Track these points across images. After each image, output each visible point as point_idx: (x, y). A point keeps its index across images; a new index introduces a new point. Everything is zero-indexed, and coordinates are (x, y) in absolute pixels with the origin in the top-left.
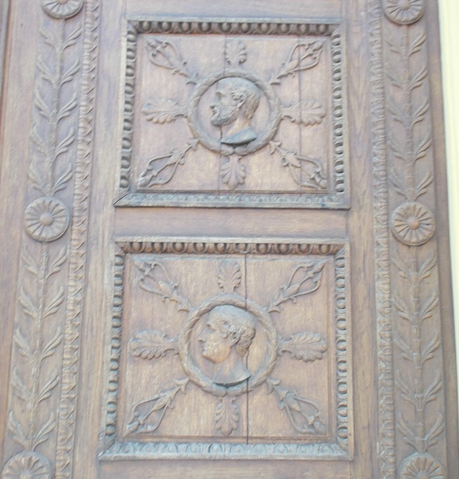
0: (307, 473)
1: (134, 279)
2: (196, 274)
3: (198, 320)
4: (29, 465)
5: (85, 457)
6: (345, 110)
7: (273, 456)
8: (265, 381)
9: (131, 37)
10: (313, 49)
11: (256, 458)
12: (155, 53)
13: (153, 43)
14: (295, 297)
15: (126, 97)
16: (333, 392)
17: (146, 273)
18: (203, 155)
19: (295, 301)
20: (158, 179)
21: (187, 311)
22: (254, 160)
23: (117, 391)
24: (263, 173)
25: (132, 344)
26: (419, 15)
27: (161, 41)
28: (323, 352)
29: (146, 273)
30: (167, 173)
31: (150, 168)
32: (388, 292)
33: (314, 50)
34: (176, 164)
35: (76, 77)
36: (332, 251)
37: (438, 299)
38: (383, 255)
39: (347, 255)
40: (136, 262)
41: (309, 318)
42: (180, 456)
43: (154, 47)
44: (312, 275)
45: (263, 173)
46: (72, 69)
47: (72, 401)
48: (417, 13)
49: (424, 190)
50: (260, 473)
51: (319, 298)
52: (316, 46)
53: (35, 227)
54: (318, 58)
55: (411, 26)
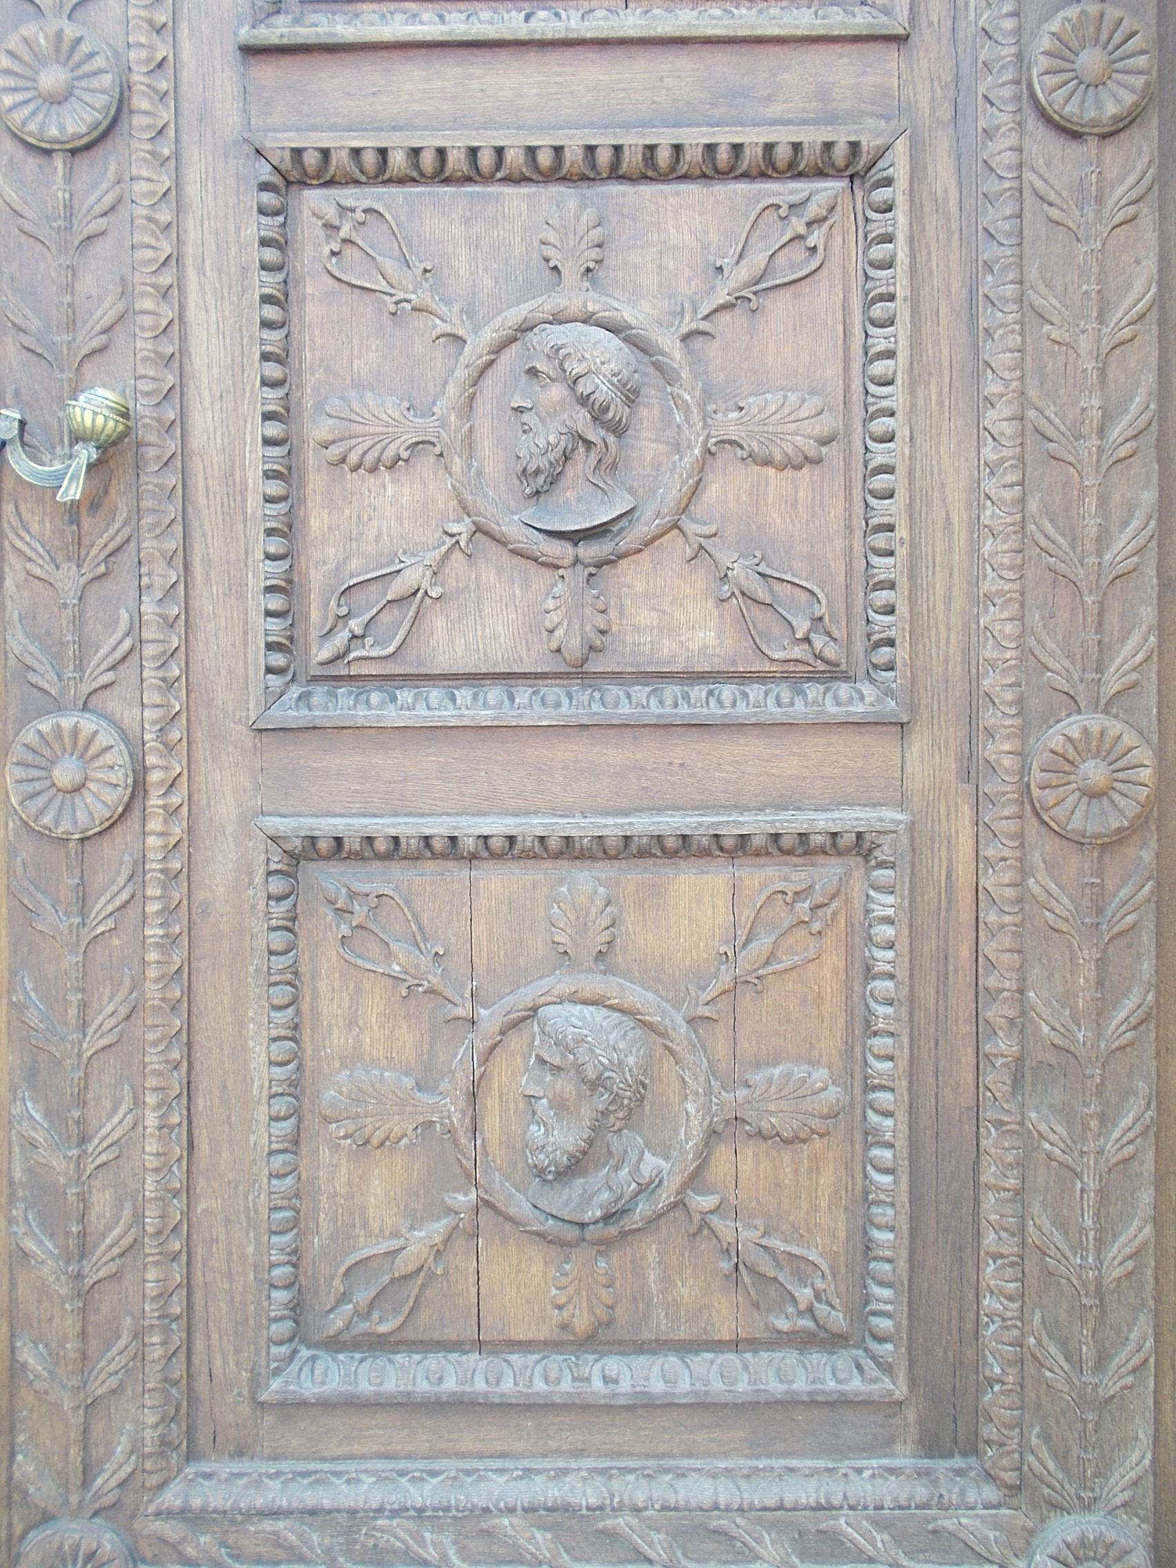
0: (786, 76)
1: (312, 246)
2: (476, 244)
3: (491, 363)
4: (58, 50)
5: (206, 49)
6: (901, 250)
7: (697, 27)
8: (675, 526)
9: (268, 198)
10: (806, 218)
11: (652, 33)
12: (336, 248)
13: (331, 213)
14: (755, 293)
15: (262, 342)
16: (857, 491)
17: (343, 233)
18: (492, 576)
19: (753, 305)
20: (369, 641)
21: (458, 340)
22: (633, 577)
23: (289, 560)
24: (672, 614)
25: (320, 430)
26: (1136, 105)
27: (349, 203)
28: (825, 441)
29: (343, 233)
30: (397, 624)
31: (344, 610)
32: (1013, 241)
33: (809, 224)
34: (419, 595)
35: (120, 335)
36: (855, 168)
37: (1153, 290)
38: (1003, 67)
39: (901, 173)
40: (330, 886)
41: (791, 363)
42: (450, 33)
43: (330, 227)
44: (802, 230)
45: (672, 614)
46: (106, 312)
47: (164, 297)
48: (1129, 99)
49: (1131, 210)
50: (662, 79)
51: (825, 298)
52: (812, 211)
53: (26, 111)
54: (821, 249)
55: (1107, 141)
